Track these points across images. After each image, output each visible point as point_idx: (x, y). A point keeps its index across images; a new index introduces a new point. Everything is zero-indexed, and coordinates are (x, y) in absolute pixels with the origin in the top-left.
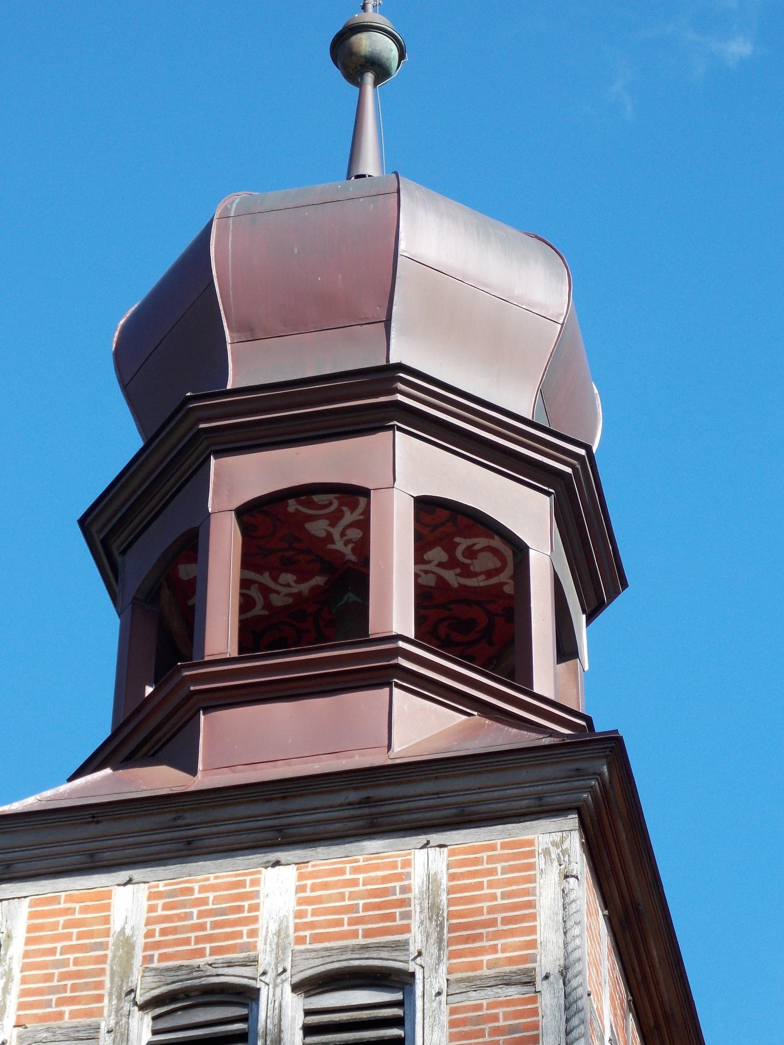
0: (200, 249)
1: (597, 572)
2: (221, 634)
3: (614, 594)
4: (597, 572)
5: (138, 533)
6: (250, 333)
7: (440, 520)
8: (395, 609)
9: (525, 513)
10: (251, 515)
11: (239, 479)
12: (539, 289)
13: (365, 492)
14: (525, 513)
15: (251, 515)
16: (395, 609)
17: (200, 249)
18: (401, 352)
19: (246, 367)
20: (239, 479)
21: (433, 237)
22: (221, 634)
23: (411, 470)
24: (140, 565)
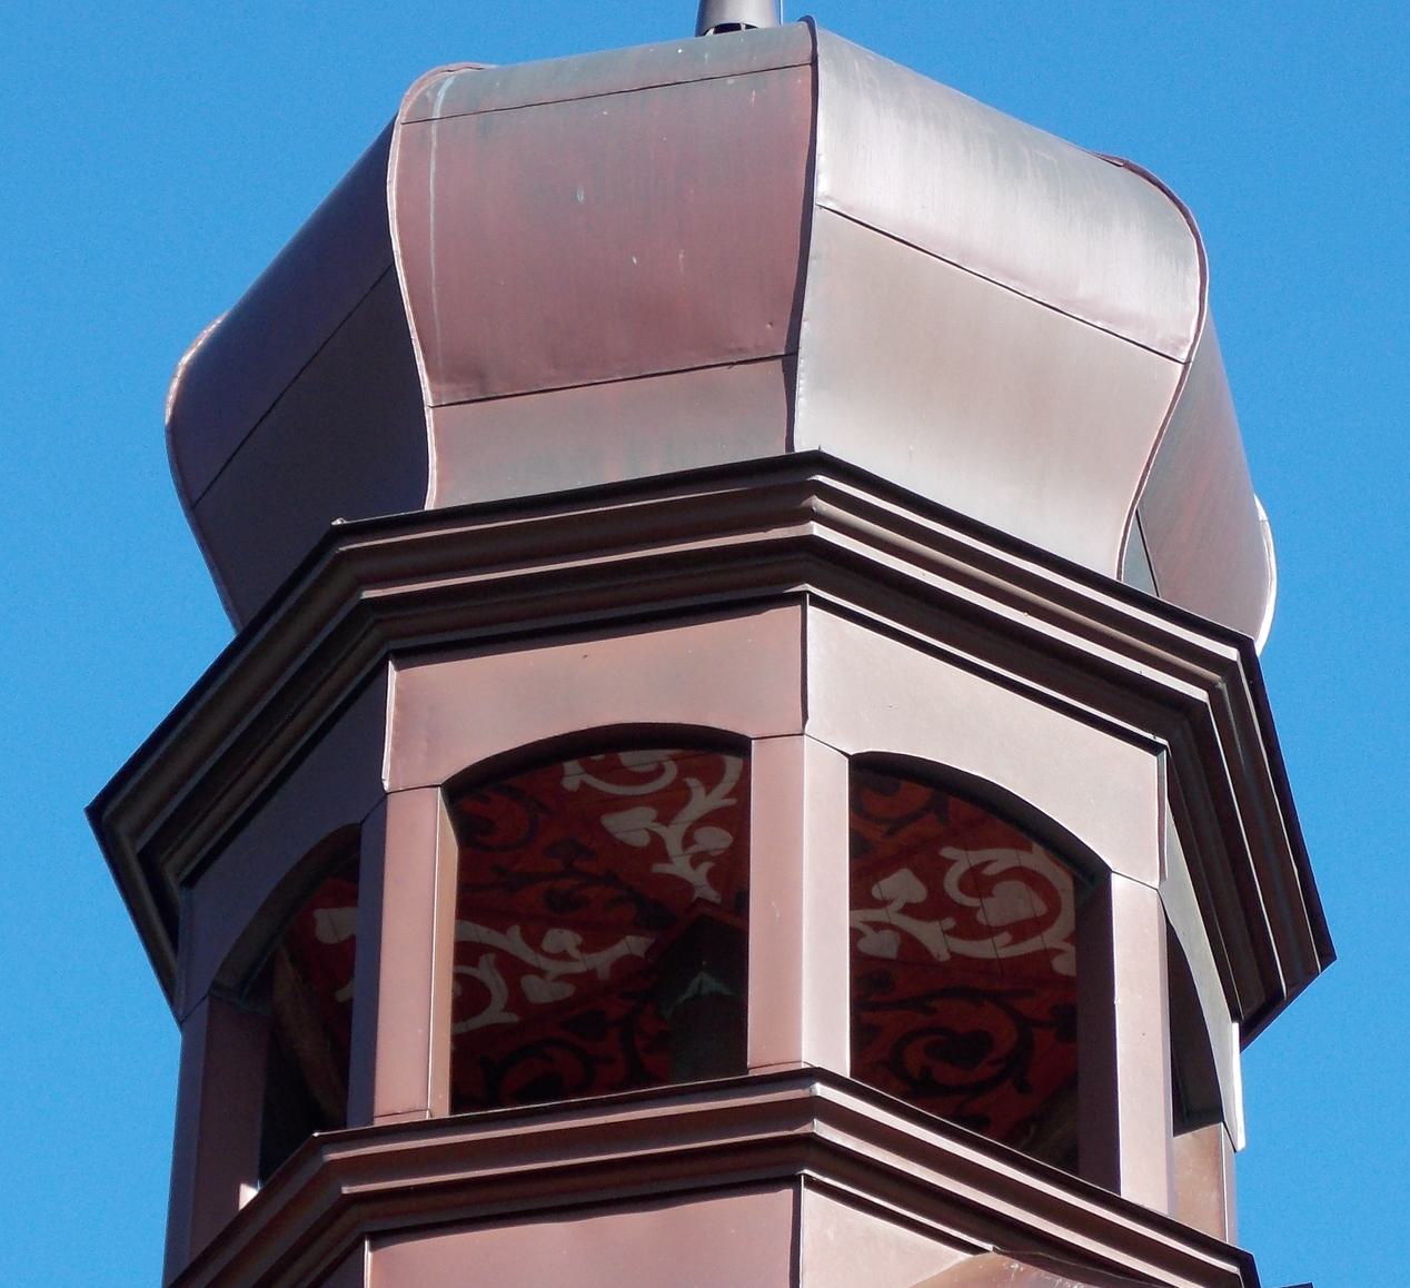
0: (357, 209)
1: (1264, 925)
2: (411, 1070)
3: (1302, 976)
4: (1264, 925)
5: (222, 838)
6: (477, 384)
7: (907, 807)
8: (806, 1009)
9: (1102, 791)
10: (477, 796)
11: (453, 715)
12: (1134, 283)
13: (738, 745)
14: (1102, 791)
15: (477, 796)
16: (806, 1009)
17: (357, 209)
18: (819, 426)
19: (469, 460)
20: (453, 715)
21: (892, 165)
22: (411, 1070)
23: (843, 695)
24: (227, 910)
